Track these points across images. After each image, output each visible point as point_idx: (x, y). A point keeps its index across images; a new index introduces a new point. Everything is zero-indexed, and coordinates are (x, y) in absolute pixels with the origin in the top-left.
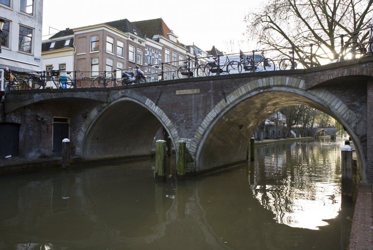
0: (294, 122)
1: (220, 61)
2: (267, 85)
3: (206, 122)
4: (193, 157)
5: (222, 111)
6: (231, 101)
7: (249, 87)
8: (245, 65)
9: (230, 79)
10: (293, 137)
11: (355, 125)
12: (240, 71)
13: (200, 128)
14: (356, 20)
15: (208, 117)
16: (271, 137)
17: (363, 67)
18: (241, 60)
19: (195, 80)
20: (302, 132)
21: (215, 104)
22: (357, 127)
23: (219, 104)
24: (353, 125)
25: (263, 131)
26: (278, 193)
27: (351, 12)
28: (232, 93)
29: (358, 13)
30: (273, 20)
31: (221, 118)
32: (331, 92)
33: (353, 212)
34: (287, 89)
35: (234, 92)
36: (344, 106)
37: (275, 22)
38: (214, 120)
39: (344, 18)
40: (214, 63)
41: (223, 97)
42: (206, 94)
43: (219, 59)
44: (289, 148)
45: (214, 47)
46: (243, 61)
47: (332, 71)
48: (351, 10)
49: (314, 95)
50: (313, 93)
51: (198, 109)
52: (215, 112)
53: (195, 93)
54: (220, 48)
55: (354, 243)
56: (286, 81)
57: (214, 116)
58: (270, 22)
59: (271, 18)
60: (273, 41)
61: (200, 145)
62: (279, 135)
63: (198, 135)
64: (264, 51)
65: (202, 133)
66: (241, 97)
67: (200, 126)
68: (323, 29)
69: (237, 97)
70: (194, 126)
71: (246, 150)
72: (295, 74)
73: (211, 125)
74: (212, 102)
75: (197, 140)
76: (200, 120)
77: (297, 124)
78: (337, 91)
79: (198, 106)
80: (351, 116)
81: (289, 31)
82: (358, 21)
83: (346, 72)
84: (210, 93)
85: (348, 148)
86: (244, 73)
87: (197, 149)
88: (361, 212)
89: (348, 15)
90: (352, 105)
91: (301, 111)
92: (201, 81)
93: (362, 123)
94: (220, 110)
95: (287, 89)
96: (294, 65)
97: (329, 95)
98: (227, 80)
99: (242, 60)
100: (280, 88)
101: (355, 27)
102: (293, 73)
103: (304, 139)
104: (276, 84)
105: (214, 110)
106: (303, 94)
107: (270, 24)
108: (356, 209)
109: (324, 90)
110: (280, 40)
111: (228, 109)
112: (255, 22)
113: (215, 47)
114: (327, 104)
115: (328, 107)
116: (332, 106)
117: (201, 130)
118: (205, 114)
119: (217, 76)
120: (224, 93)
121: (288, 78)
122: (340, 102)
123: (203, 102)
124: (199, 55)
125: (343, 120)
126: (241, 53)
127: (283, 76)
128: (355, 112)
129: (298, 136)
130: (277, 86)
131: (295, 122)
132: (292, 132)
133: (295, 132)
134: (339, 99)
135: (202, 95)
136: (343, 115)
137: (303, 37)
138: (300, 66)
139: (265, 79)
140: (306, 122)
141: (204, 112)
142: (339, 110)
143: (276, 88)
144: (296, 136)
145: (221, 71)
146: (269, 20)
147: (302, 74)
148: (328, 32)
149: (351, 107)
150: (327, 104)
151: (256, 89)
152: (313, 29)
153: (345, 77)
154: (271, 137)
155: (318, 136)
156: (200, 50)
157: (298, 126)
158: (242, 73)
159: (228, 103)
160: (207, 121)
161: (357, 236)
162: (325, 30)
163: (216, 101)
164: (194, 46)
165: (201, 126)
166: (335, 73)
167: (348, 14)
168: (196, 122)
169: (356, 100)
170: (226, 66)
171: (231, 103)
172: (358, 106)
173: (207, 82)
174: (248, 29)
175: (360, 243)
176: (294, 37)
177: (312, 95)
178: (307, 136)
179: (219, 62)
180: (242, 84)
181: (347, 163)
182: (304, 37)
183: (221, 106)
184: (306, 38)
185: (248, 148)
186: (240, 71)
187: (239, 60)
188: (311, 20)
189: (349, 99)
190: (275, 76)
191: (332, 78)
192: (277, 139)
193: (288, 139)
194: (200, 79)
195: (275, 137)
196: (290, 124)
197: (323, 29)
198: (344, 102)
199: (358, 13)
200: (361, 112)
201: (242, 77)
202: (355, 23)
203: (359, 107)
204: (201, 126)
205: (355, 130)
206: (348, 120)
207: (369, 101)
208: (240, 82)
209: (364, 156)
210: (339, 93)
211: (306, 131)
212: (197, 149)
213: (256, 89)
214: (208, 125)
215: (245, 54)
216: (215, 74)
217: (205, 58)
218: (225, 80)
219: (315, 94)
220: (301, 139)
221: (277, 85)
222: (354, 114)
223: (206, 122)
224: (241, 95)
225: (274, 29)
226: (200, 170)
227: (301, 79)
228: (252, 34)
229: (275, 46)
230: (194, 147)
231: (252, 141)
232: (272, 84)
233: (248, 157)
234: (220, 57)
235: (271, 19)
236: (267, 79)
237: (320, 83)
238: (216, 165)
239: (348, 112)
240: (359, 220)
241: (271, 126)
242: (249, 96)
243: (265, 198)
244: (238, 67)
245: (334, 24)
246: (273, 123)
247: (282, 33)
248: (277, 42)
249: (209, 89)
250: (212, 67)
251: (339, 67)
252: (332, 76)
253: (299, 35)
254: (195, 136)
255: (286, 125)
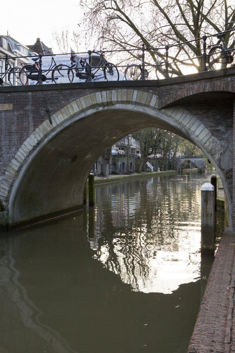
0: (151, 151)
1: (42, 63)
2: (108, 101)
3: (23, 152)
4: (4, 204)
5: (45, 136)
6: (58, 123)
7: (83, 103)
8: (78, 71)
9: (56, 90)
10: (150, 171)
11: (219, 156)
12: (71, 79)
13: (14, 161)
14: (228, 16)
15: (24, 145)
16: (120, 171)
17: (228, 81)
18: (72, 64)
19: (5, 91)
20: (162, 164)
21: (36, 126)
22: (222, 159)
23: (41, 127)
24: (217, 156)
25: (109, 164)
26: (130, 250)
27: (222, 4)
28: (59, 111)
29: (230, 6)
30: (121, 7)
31: (45, 147)
32: (191, 112)
33: (211, 269)
34: (134, 108)
35: (62, 110)
36: (206, 131)
37: (123, 10)
38: (34, 149)
39: (214, 11)
40: (34, 65)
41: (47, 117)
42: (22, 112)
43: (41, 61)
44: (145, 183)
45: (38, 40)
46: (75, 65)
47: (192, 85)
48: (223, 1)
49: (170, 116)
50: (168, 113)
51: (10, 133)
52: (35, 137)
53: (5, 109)
54: (47, 42)
55: (205, 309)
56: (134, 96)
57: (35, 144)
58: (116, 10)
59: (118, 4)
60: (121, 37)
61: (14, 186)
62: (131, 168)
63: (12, 171)
64: (104, 52)
65: (16, 169)
66: (72, 117)
67: (13, 158)
68: (187, 24)
69: (66, 117)
70: (5, 158)
71: (82, 190)
72: (145, 86)
73: (30, 157)
74: (31, 123)
75: (10, 179)
76: (13, 149)
77: (155, 153)
78: (198, 111)
79: (11, 129)
80: (214, 144)
81: (143, 24)
82: (230, 17)
83: (208, 87)
84: (28, 110)
85: (209, 187)
86: (79, 82)
87: (10, 192)
88: (219, 269)
89: (219, 8)
90: (217, 130)
91: (159, 135)
92: (15, 92)
93: (228, 153)
94: (42, 135)
95: (134, 108)
96: (144, 72)
97: (189, 116)
98: (53, 92)
99: (74, 64)
100: (126, 105)
101: (226, 25)
102: (143, 84)
103: (164, 173)
104: (120, 100)
105: (34, 134)
106: (155, 114)
107: (116, 12)
108: (214, 265)
109: (183, 110)
110: (130, 37)
111: (54, 133)
112: (96, 8)
113: (41, 41)
114: (186, 128)
115: (188, 133)
116: (191, 131)
117: (15, 165)
118: (21, 141)
119: (39, 86)
120: (47, 111)
121: (136, 92)
122: (202, 126)
123: (18, 123)
124: (17, 51)
125: (205, 150)
126: (72, 53)
127: (129, 89)
128: (220, 140)
129: (156, 170)
130: (122, 102)
131: (153, 150)
132: (148, 164)
133: (153, 165)
134: (200, 122)
135: (16, 113)
136: (205, 143)
137: (162, 33)
138: (153, 75)
139: (105, 92)
140: (167, 150)
141: (19, 137)
142: (201, 137)
143: (121, 105)
144: (153, 169)
145: (44, 78)
146: (115, 7)
147: (154, 86)
148: (194, 29)
149: (214, 132)
150: (186, 128)
151: (93, 107)
152: (174, 24)
153: (207, 92)
154: (120, 171)
155: (182, 169)
156: (17, 44)
157: (156, 156)
158: (74, 82)
159: (54, 125)
160: (24, 151)
161: (210, 300)
162: (189, 26)
163: (37, 122)
164: (8, 37)
165: (16, 159)
166: (196, 88)
167: (219, 6)
168: (8, 153)
169: (221, 124)
170: (51, 72)
171: (58, 126)
172: (223, 131)
173: (24, 94)
174: (85, 18)
175: (212, 309)
176: (150, 33)
177: (167, 116)
178: (168, 169)
179: (41, 65)
180: (74, 99)
181: (208, 206)
182: (163, 34)
183: (44, 129)
184: (166, 35)
185: (85, 189)
186: (71, 80)
187: (69, 64)
188: (171, 10)
189: (213, 122)
190: (119, 89)
191: (191, 94)
192: (128, 174)
193: (142, 174)
194: (13, 89)
195: (126, 171)
196: (145, 154)
197: (187, 24)
198: (207, 126)
199: (230, 6)
200: (227, 140)
201: (73, 89)
202: (227, 19)
203: (224, 133)
204: (16, 159)
205: (219, 162)
206: (211, 150)
207: (234, 127)
208: (71, 95)
209: (230, 196)
210: (200, 114)
211: (167, 163)
212: (10, 192)
213: (93, 107)
214: (26, 156)
215: (78, 55)
216: (35, 82)
217: (27, 58)
218: (49, 92)
219: (170, 114)
220: (160, 173)
221: (121, 101)
222: (218, 142)
223: (23, 152)
224: (72, 114)
225: (123, 20)
226: (14, 222)
227: (153, 93)
228: (91, 26)
229: (123, 44)
230: (5, 189)
231: (91, 178)
232: (114, 99)
233: (85, 202)
234: (43, 57)
235: (117, 6)
236: (108, 92)
237: (177, 100)
238: (38, 214)
239: (211, 140)
240: (215, 279)
241: (119, 155)
242: (83, 115)
243: (113, 257)
244: (68, 73)
245: (201, 19)
246: (122, 152)
247: (132, 26)
248: (127, 39)
249: (26, 105)
250: (31, 73)
251: (200, 80)
252: (192, 91)
253: (156, 30)
254: (6, 173)
255: (140, 155)
